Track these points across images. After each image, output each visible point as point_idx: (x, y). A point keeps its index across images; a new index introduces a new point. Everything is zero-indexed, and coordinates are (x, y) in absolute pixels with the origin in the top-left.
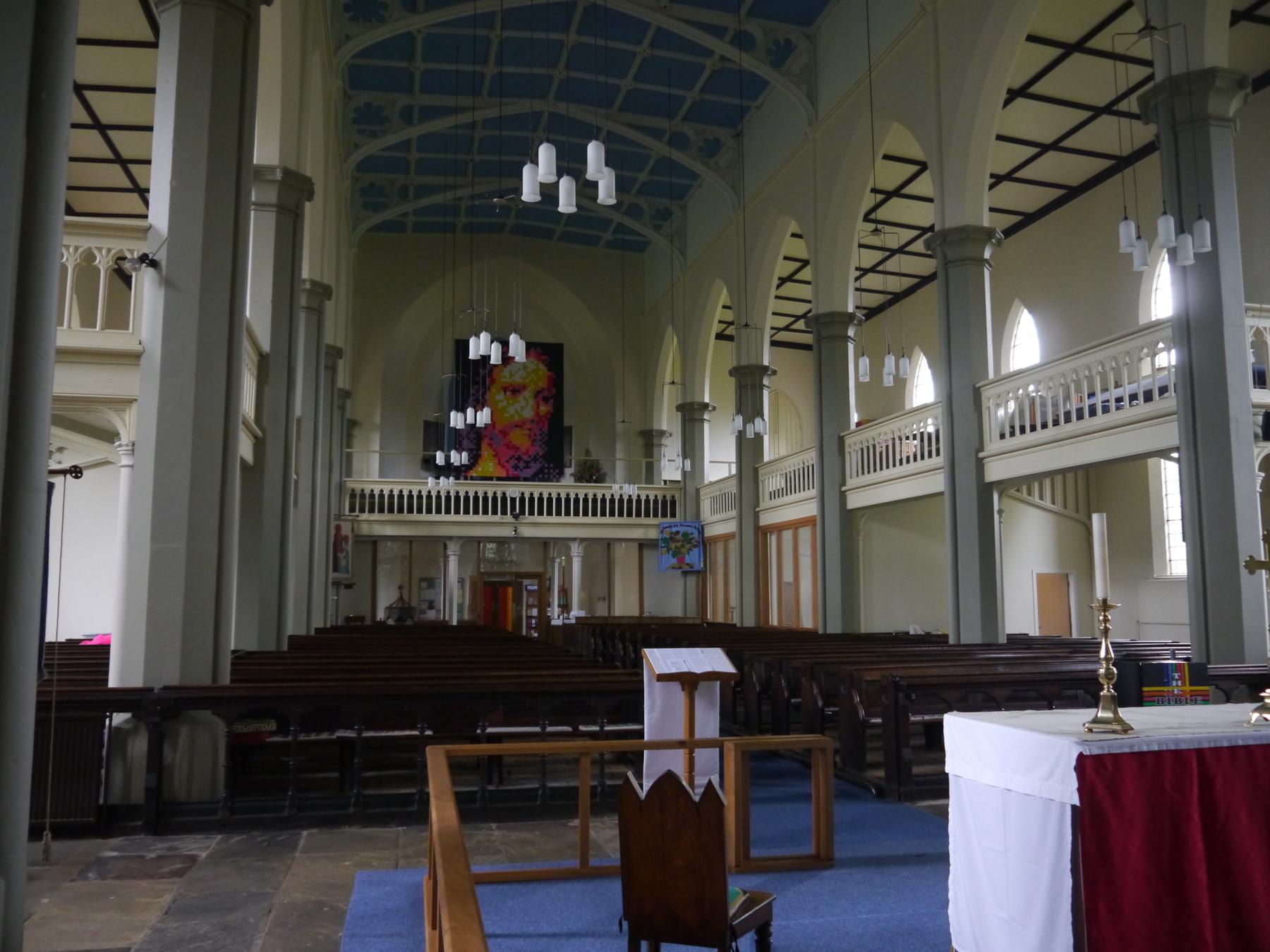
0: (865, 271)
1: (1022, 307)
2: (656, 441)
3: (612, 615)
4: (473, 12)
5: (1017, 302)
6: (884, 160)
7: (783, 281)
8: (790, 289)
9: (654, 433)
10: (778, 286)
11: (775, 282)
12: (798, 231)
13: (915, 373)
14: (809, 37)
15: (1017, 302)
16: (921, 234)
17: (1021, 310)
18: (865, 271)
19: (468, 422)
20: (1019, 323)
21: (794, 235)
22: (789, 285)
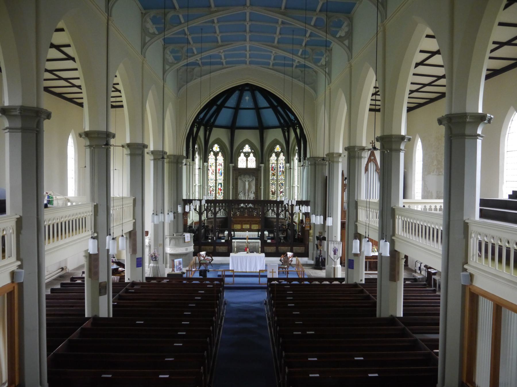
0: (501, 45)
1: (515, 112)
2: (335, 160)
3: (336, 277)
4: (186, 63)
5: (512, 108)
6: (426, 38)
7: (417, 65)
8: (422, 69)
9: (334, 156)
10: (416, 67)
11: (414, 65)
12: (431, 33)
13: (508, 124)
14: (349, 18)
15: (512, 108)
16: (437, 79)
17: (514, 114)
18: (501, 45)
19: (160, 221)
20: (512, 121)
21: (428, 36)
22: (420, 67)
